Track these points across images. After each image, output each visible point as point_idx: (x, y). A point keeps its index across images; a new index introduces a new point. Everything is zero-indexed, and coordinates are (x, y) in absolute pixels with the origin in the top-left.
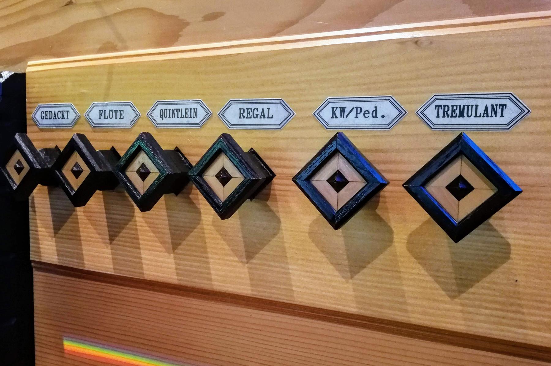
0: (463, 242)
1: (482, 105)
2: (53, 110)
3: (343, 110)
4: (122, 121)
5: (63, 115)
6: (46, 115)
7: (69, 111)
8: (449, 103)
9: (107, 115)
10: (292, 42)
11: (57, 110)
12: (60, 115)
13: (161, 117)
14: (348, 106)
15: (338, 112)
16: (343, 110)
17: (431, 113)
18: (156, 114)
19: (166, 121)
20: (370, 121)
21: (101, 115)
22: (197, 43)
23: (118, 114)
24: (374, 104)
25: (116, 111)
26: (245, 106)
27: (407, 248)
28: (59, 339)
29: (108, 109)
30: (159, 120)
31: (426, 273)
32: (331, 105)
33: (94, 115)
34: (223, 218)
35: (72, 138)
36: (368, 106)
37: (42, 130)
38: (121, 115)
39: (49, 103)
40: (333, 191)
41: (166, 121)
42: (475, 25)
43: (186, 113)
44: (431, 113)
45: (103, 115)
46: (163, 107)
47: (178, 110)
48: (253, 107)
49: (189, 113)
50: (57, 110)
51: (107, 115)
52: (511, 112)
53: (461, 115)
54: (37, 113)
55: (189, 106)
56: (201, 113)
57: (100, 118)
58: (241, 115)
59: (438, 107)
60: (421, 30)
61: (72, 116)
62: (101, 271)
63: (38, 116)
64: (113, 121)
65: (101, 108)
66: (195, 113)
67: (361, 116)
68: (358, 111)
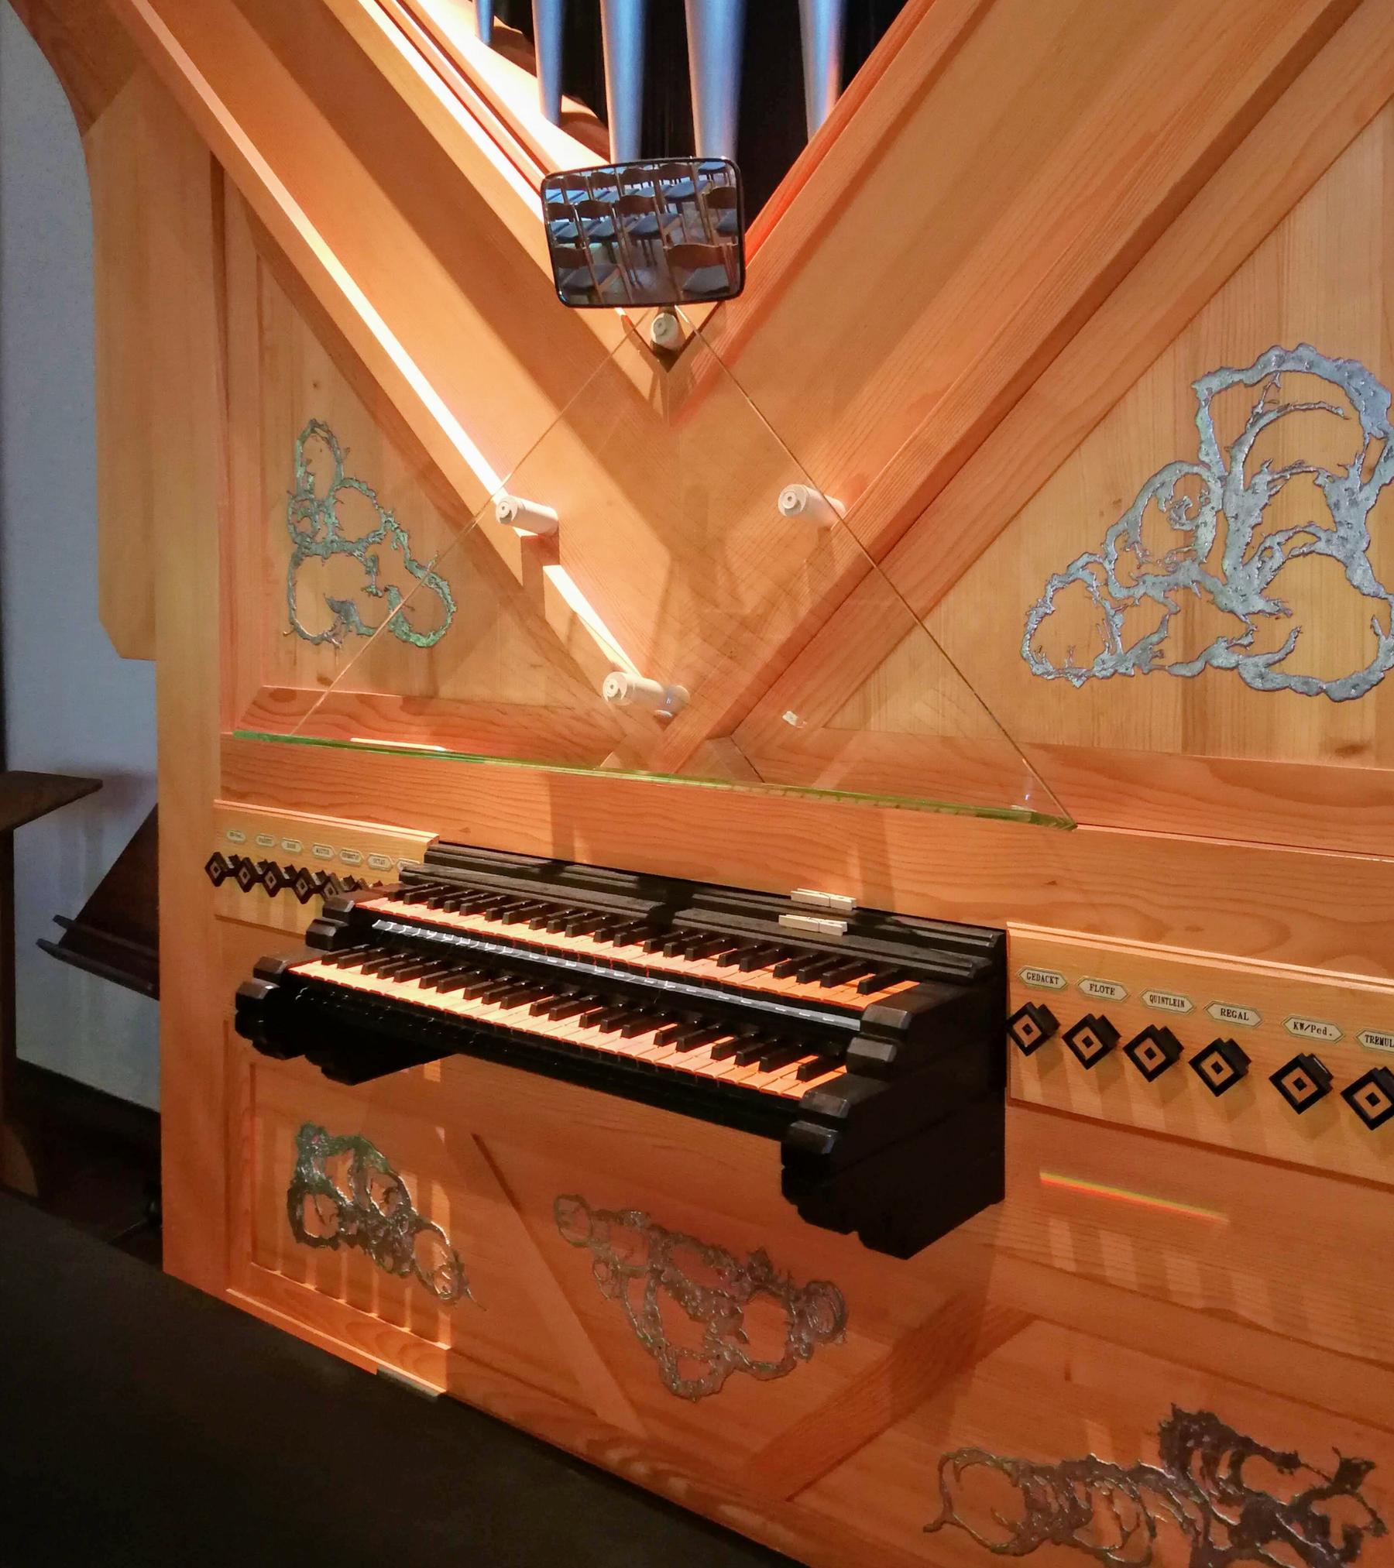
1: (1238, 1011)
2: (1041, 974)
3: (1302, 1025)
4: (1112, 996)
7: (1384, 1529)
8: (1374, 1035)
9: (1098, 989)
11: (1045, 975)
12: (1049, 979)
13: (1152, 1001)
14: (1306, 1024)
15: (1298, 1026)
16: (1302, 1025)
17: (1362, 1038)
18: (1147, 997)
19: (1154, 1004)
20: (1321, 1036)
22: (1184, 946)
23: (1109, 991)
24: (1324, 1026)
25: (1107, 988)
26: (1032, 972)
27: (292, 557)
28: (1046, 1225)
29: (1099, 985)
30: (1149, 1003)
32: (1027, 971)
33: (1085, 986)
35: (1030, 822)
36: (1322, 1027)
37: (1026, 987)
40: (1296, 1089)
41: (1154, 1004)
44: (1362, 1038)
48: (1232, 1009)
50: (1045, 975)
51: (1098, 989)
53: (1382, 1043)
54: (684, 916)
56: (1188, 1006)
58: (1222, 1013)
59: (1367, 1036)
61: (1061, 983)
62: (857, 76)
63: (1024, 976)
64: (1105, 994)
65: (1092, 982)
67: (1315, 1031)
68: (1313, 1028)
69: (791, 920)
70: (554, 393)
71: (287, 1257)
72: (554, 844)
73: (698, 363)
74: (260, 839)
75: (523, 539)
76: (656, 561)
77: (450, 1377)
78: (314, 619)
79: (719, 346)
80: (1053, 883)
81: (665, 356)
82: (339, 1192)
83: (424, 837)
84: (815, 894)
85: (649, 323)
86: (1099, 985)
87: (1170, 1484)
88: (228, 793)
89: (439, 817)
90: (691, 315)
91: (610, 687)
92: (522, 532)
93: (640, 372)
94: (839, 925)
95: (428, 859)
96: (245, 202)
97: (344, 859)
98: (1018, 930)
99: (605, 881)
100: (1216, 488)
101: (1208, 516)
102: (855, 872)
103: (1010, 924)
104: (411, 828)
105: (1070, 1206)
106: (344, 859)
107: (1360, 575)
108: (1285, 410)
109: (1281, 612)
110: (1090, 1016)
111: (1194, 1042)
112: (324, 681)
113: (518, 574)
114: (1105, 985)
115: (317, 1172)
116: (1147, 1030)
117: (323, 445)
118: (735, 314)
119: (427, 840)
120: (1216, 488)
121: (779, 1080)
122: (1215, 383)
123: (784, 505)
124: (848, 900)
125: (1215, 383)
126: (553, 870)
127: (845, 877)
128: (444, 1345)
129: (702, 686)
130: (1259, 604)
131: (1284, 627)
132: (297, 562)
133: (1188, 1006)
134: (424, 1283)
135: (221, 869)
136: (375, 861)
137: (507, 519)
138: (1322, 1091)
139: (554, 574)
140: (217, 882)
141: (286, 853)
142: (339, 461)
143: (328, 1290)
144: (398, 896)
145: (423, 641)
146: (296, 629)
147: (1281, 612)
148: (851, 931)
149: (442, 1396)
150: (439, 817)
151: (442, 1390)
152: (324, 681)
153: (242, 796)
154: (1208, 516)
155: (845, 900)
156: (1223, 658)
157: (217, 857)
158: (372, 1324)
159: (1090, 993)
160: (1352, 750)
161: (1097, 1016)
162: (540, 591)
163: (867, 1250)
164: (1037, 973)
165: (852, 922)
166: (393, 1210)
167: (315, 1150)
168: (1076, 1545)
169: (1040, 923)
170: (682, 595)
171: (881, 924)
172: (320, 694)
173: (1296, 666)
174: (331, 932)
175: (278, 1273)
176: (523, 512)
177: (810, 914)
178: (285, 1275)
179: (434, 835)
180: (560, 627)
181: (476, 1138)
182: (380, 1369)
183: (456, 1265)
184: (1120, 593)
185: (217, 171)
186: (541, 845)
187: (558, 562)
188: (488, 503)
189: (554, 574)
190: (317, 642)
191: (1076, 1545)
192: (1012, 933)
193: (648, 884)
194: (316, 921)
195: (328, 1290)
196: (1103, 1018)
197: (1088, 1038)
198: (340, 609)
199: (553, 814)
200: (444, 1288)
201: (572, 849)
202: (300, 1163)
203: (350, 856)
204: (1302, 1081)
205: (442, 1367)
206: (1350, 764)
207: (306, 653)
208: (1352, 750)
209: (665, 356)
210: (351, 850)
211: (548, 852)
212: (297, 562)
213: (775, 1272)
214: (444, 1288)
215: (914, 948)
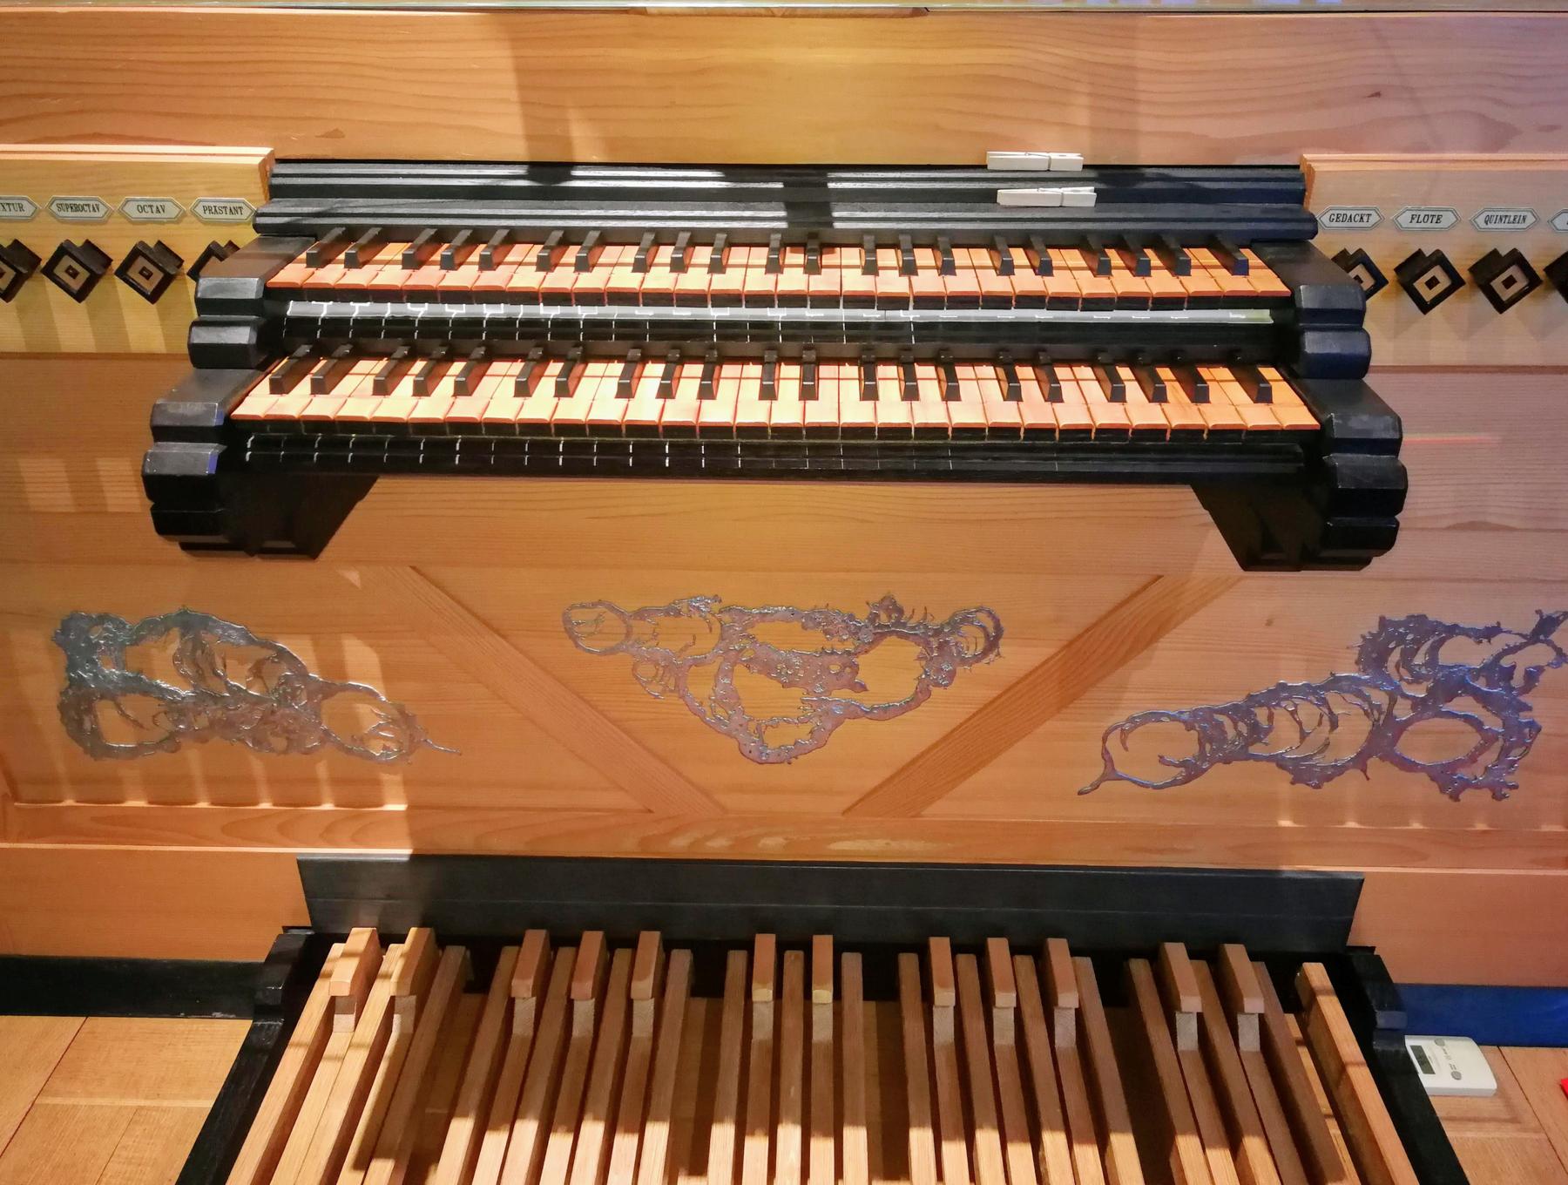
0: (1358, 248)
5: (1362, 218)
6: (1338, 218)
10: (994, 1095)
12: (1358, 218)
15: (1365, 218)
16: (158, 211)
19: (1490, 226)
21: (1413, 218)
25: (225, 207)
30: (1483, 225)
31: (1215, 261)
32: (202, 204)
34: (1360, 250)
38: (1438, 219)
39: (941, 191)
42: (1000, 1097)
43: (1514, 219)
45: (1416, 219)
46: (1490, 214)
47: (1506, 216)
49: (1517, 220)
50: (82, 203)
52: (1374, 218)
55: (1519, 214)
57: (1411, 222)
60: (962, 1099)
65: (1414, 213)
66: (1524, 219)
69: (1007, 195)
71: (78, 781)
72: (530, 138)
74: (205, 209)
77: (414, 835)
80: (1378, 94)
82: (164, 686)
83: (253, 155)
84: (1021, 155)
86: (1423, 214)
87: (1366, 682)
89: (266, 118)
97: (63, 214)
98: (1323, 163)
99: (1272, 185)
103: (1307, 156)
104: (214, 145)
106: (63, 214)
110: (215, 244)
114: (1430, 213)
115: (113, 672)
116: (209, 248)
119: (257, 161)
121: (349, 400)
124: (1074, 156)
133: (1530, 219)
134: (349, 751)
136: (205, 209)
138: (167, 280)
149: (413, 857)
150: (266, 118)
151: (409, 851)
155: (1072, 159)
158: (266, 815)
159: (1411, 225)
161: (151, 244)
163: (1371, 565)
164: (1342, 212)
165: (1101, 186)
166: (273, 683)
167: (98, 644)
168: (1257, 758)
169: (1347, 150)
171: (566, 180)
175: (69, 802)
177: (1043, 184)
178: (77, 802)
179: (266, 151)
182: (300, 858)
183: (402, 719)
191: (1257, 758)
192: (1317, 167)
194: (195, 324)
196: (88, 243)
197: (144, 269)
199: (521, 87)
200: (385, 748)
201: (567, 142)
202: (72, 666)
203: (76, 208)
204: (73, 269)
205: (403, 828)
210: (79, 198)
213: (907, 614)
214: (385, 748)
215: (1181, 206)
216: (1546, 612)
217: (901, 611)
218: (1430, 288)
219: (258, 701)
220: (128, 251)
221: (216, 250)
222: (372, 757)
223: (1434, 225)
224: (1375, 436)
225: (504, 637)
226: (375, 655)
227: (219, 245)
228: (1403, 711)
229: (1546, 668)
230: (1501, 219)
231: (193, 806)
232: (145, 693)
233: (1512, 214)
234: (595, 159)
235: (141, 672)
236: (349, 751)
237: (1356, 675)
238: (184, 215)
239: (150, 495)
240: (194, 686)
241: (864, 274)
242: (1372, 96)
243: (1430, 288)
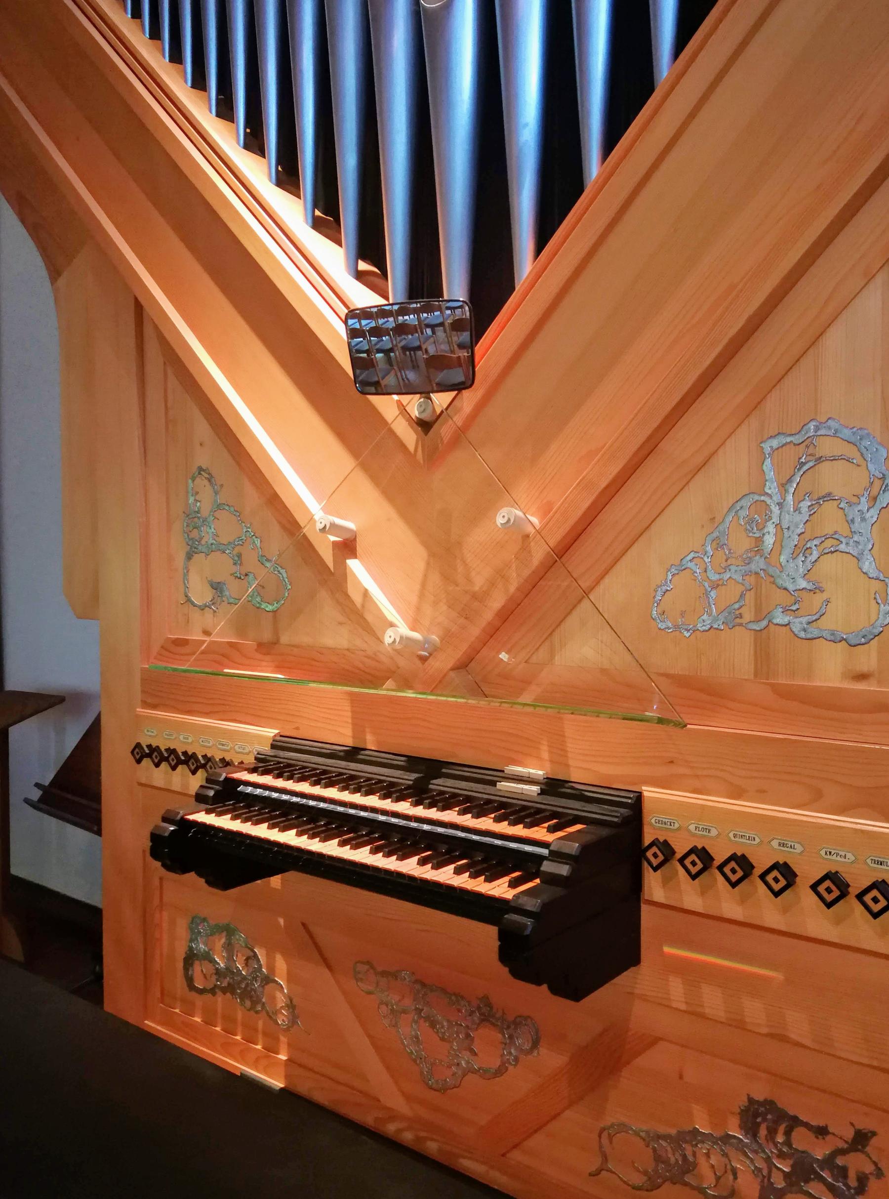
16: (671, 825)
19: (736, 839)
32: (655, 818)
65: (696, 825)
70: (354, 450)
71: (184, 1001)
72: (354, 737)
73: (445, 430)
75: (334, 542)
76: (418, 556)
77: (287, 1077)
78: (200, 593)
79: (458, 420)
80: (672, 762)
81: (424, 426)
83: (271, 732)
84: (520, 769)
85: (414, 404)
86: (701, 827)
87: (746, 1145)
88: (146, 704)
90: (441, 400)
91: (389, 637)
92: (333, 538)
93: (408, 436)
94: (535, 789)
95: (273, 747)
96: (156, 327)
98: (650, 792)
100: (776, 510)
101: (771, 528)
102: (545, 755)
103: (644, 788)
105: (682, 968)
107: (868, 565)
108: (819, 460)
109: (817, 589)
110: (695, 847)
111: (761, 863)
112: (207, 633)
113: (331, 565)
114: (705, 827)
117: (206, 482)
118: (469, 399)
120: (776, 510)
121: (497, 887)
122: (775, 443)
123: (500, 521)
124: (541, 773)
125: (775, 443)
126: (353, 754)
127: (539, 758)
128: (283, 1057)
129: (447, 636)
130: (803, 584)
131: (819, 598)
132: (189, 557)
133: (757, 840)
134: (270, 1017)
135: (141, 753)
136: (239, 748)
137: (323, 530)
139: (354, 565)
140: (139, 761)
141: (182, 743)
142: (216, 493)
143: (209, 1022)
144: (253, 770)
145: (270, 608)
146: (189, 600)
147: (817, 589)
148: (543, 792)
151: (282, 1086)
152: (207, 633)
153: (154, 707)
154: (771, 528)
155: (539, 773)
156: (780, 618)
157: (138, 745)
158: (237, 1043)
159: (695, 832)
160: (862, 677)
162: (345, 576)
166: (251, 970)
168: (686, 1184)
169: (663, 788)
170: (435, 578)
172: (204, 642)
173: (827, 623)
174: (211, 793)
175: (177, 1011)
176: (333, 525)
179: (277, 731)
180: (357, 599)
181: (304, 925)
183: (291, 1006)
184: (714, 577)
185: (139, 308)
186: (344, 737)
187: (356, 557)
188: (311, 519)
189: (354, 565)
190: (202, 608)
191: (686, 1184)
192: (645, 794)
193: (413, 762)
195: (209, 1022)
196: (704, 848)
197: (776, 877)
198: (217, 587)
199: (353, 718)
201: (365, 741)
202: (191, 941)
203: (223, 745)
205: (282, 1071)
206: (861, 686)
207: (195, 615)
208: (862, 677)
209: (424, 426)
210: (224, 741)
211: (350, 742)
212: (189, 557)
213: (494, 1010)
215: (583, 804)
216: (859, 1126)
217: (491, 1008)
218: (658, 856)
219: (244, 978)
220: (688, 849)
221: (830, 875)
222: (278, 1024)
223: (707, 834)
224: (525, 908)
225: (329, 967)
226: (285, 966)
227: (779, 863)
228: (779, 1183)
229: (869, 1176)
230: (742, 837)
231: (275, 1055)
232: (211, 962)
233: (748, 835)
234: (373, 748)
235: (210, 950)
236: (270, 1017)
237: (741, 1137)
238: (250, 752)
239: (152, 841)
240: (226, 963)
241: (458, 814)
242: (669, 762)
243: (658, 856)
